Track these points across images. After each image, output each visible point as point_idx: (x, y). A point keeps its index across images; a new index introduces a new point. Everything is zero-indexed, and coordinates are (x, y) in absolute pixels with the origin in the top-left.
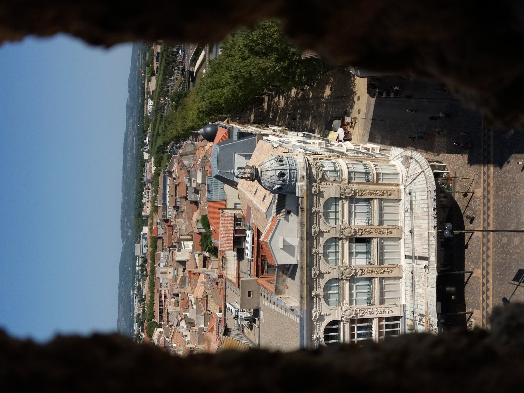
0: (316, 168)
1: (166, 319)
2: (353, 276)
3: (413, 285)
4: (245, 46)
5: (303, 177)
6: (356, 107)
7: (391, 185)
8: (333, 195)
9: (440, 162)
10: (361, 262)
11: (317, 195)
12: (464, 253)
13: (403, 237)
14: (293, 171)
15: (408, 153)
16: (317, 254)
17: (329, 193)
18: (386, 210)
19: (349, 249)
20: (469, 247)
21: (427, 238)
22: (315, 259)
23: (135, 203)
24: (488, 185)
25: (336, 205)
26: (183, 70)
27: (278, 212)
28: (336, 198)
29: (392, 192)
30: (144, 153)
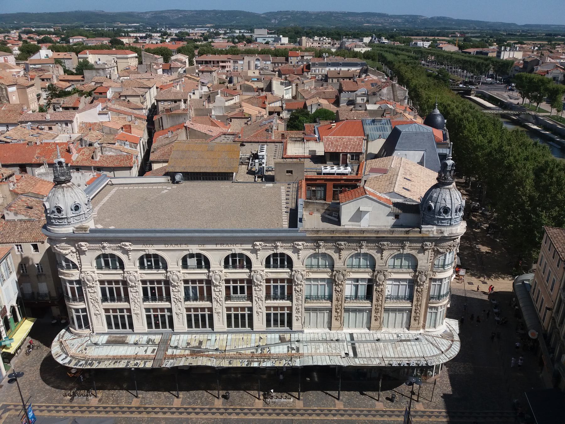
1: (205, 69)
2: (336, 282)
3: (325, 341)
4: (546, 162)
5: (442, 233)
6: (474, 279)
8: (420, 263)
9: (441, 369)
10: (348, 290)
11: (422, 247)
12: (355, 390)
13: (371, 332)
14: (449, 222)
15: (457, 338)
16: (361, 247)
17: (422, 260)
18: (399, 315)
19: (362, 279)
20: (363, 397)
21: (376, 356)
22: (355, 244)
23: (308, 27)
24: (430, 416)
25: (409, 266)
26: (471, 83)
27: (396, 205)
28: (417, 266)
29: (417, 321)
30: (370, 38)
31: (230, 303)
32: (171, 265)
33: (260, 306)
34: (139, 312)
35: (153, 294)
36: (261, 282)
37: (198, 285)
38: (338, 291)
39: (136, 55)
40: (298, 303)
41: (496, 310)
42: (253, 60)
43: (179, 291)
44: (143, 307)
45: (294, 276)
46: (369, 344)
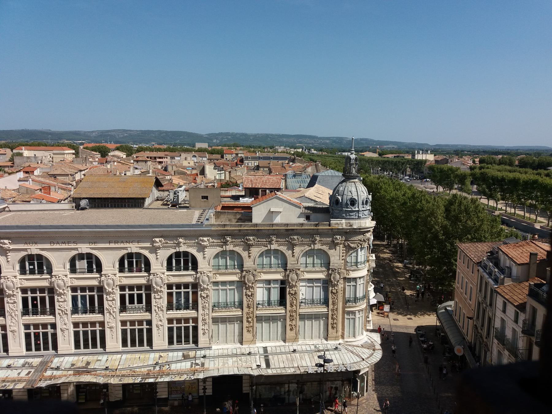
0: (360, 241)
2: (246, 284)
3: (236, 355)
7: (343, 329)
8: (332, 259)
9: (367, 391)
10: (260, 294)
13: (287, 344)
14: (357, 214)
15: (378, 347)
18: (315, 323)
21: (291, 366)
25: (321, 264)
28: (330, 263)
31: (126, 316)
32: (57, 268)
33: (161, 318)
34: (15, 329)
35: (35, 306)
36: (161, 287)
37: (88, 293)
38: (249, 296)
39: (74, 151)
40: (204, 313)
41: (423, 339)
42: (189, 156)
43: (65, 301)
44: (21, 322)
45: (199, 278)
46: (284, 356)
